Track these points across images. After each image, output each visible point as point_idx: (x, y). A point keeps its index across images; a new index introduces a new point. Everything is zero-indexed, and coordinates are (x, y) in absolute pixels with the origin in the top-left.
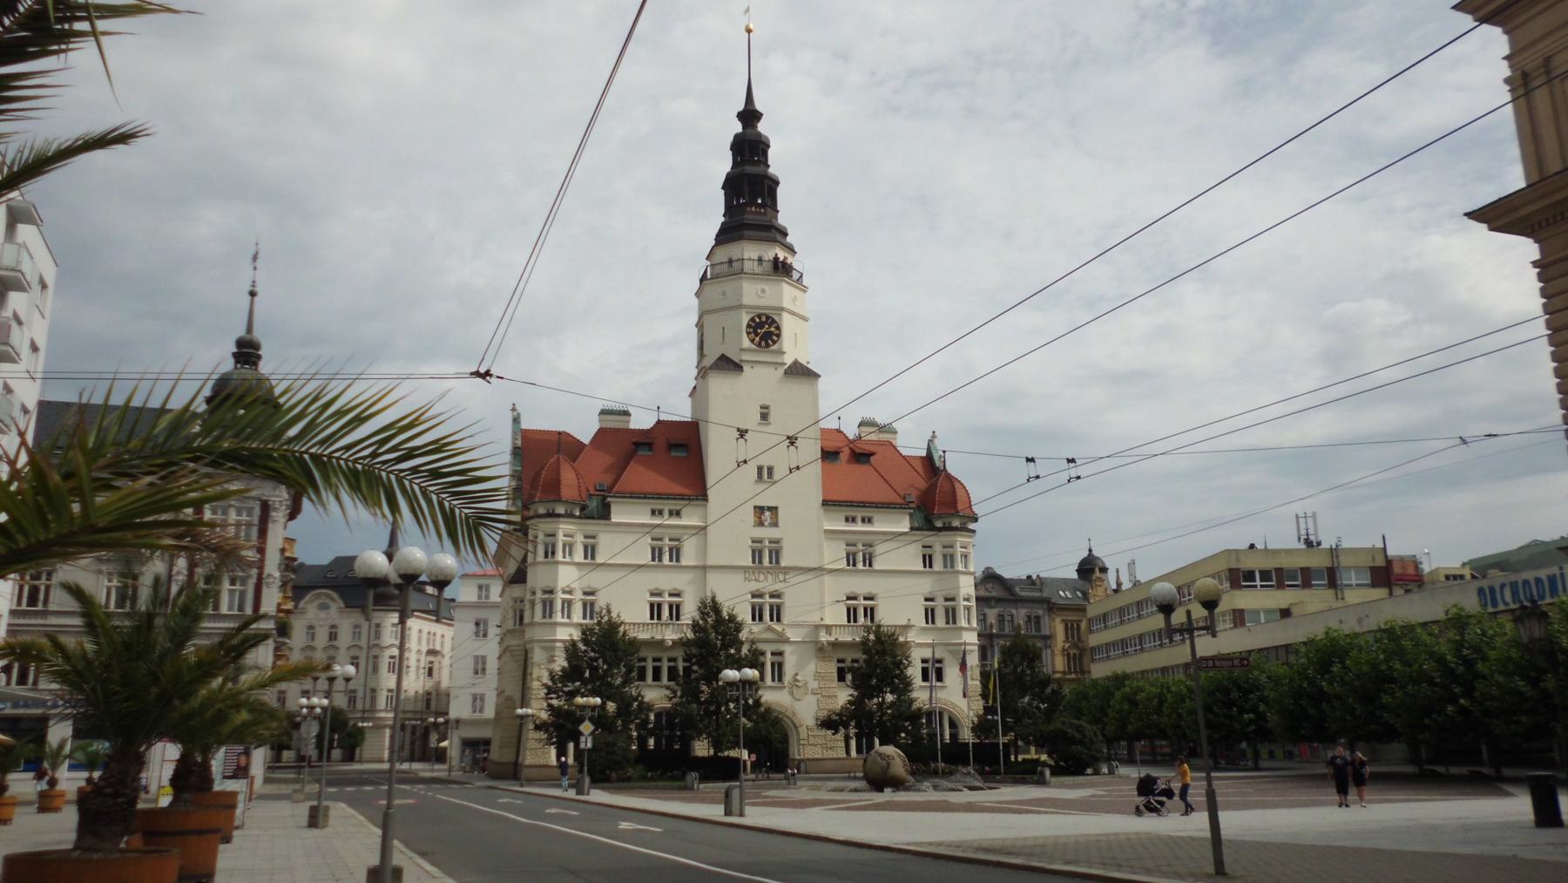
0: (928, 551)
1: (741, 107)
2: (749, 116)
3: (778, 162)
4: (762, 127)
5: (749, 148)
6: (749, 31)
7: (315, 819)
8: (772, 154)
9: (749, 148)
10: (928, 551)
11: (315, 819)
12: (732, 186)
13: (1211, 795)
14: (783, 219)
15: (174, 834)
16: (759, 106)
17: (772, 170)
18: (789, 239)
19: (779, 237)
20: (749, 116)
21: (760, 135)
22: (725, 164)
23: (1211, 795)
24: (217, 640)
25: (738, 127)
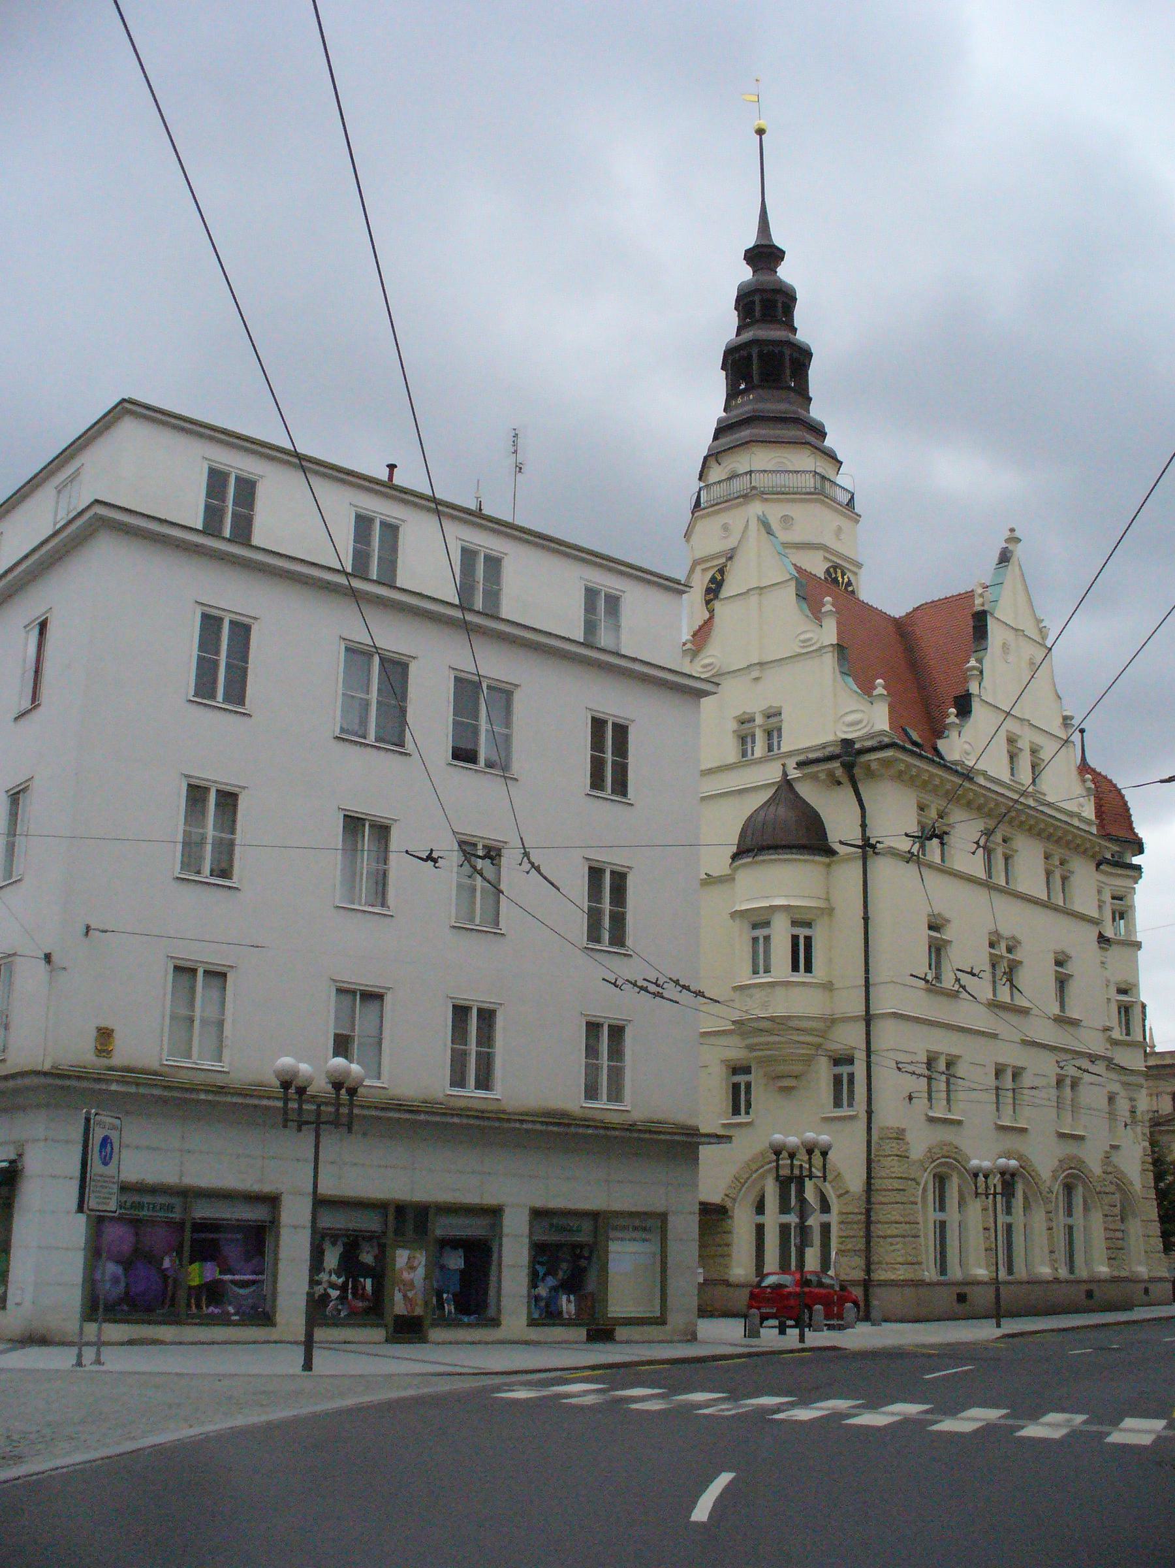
0: (802, 932)
1: (751, 241)
2: (764, 255)
3: (809, 325)
4: (786, 272)
5: (766, 302)
6: (760, 132)
7: (105, 1035)
8: (800, 316)
9: (766, 302)
10: (802, 932)
11: (105, 1035)
12: (738, 363)
13: (792, 1170)
14: (816, 412)
15: (57, 503)
16: (778, 240)
17: (802, 336)
18: (828, 442)
19: (810, 438)
20: (764, 255)
21: (780, 281)
22: (725, 326)
23: (792, 1170)
24: (769, 794)
25: (746, 273)
